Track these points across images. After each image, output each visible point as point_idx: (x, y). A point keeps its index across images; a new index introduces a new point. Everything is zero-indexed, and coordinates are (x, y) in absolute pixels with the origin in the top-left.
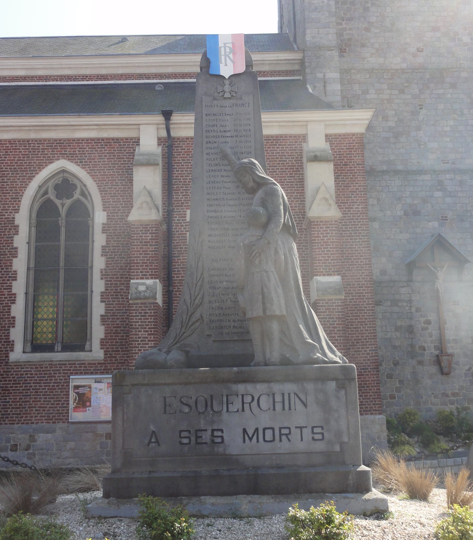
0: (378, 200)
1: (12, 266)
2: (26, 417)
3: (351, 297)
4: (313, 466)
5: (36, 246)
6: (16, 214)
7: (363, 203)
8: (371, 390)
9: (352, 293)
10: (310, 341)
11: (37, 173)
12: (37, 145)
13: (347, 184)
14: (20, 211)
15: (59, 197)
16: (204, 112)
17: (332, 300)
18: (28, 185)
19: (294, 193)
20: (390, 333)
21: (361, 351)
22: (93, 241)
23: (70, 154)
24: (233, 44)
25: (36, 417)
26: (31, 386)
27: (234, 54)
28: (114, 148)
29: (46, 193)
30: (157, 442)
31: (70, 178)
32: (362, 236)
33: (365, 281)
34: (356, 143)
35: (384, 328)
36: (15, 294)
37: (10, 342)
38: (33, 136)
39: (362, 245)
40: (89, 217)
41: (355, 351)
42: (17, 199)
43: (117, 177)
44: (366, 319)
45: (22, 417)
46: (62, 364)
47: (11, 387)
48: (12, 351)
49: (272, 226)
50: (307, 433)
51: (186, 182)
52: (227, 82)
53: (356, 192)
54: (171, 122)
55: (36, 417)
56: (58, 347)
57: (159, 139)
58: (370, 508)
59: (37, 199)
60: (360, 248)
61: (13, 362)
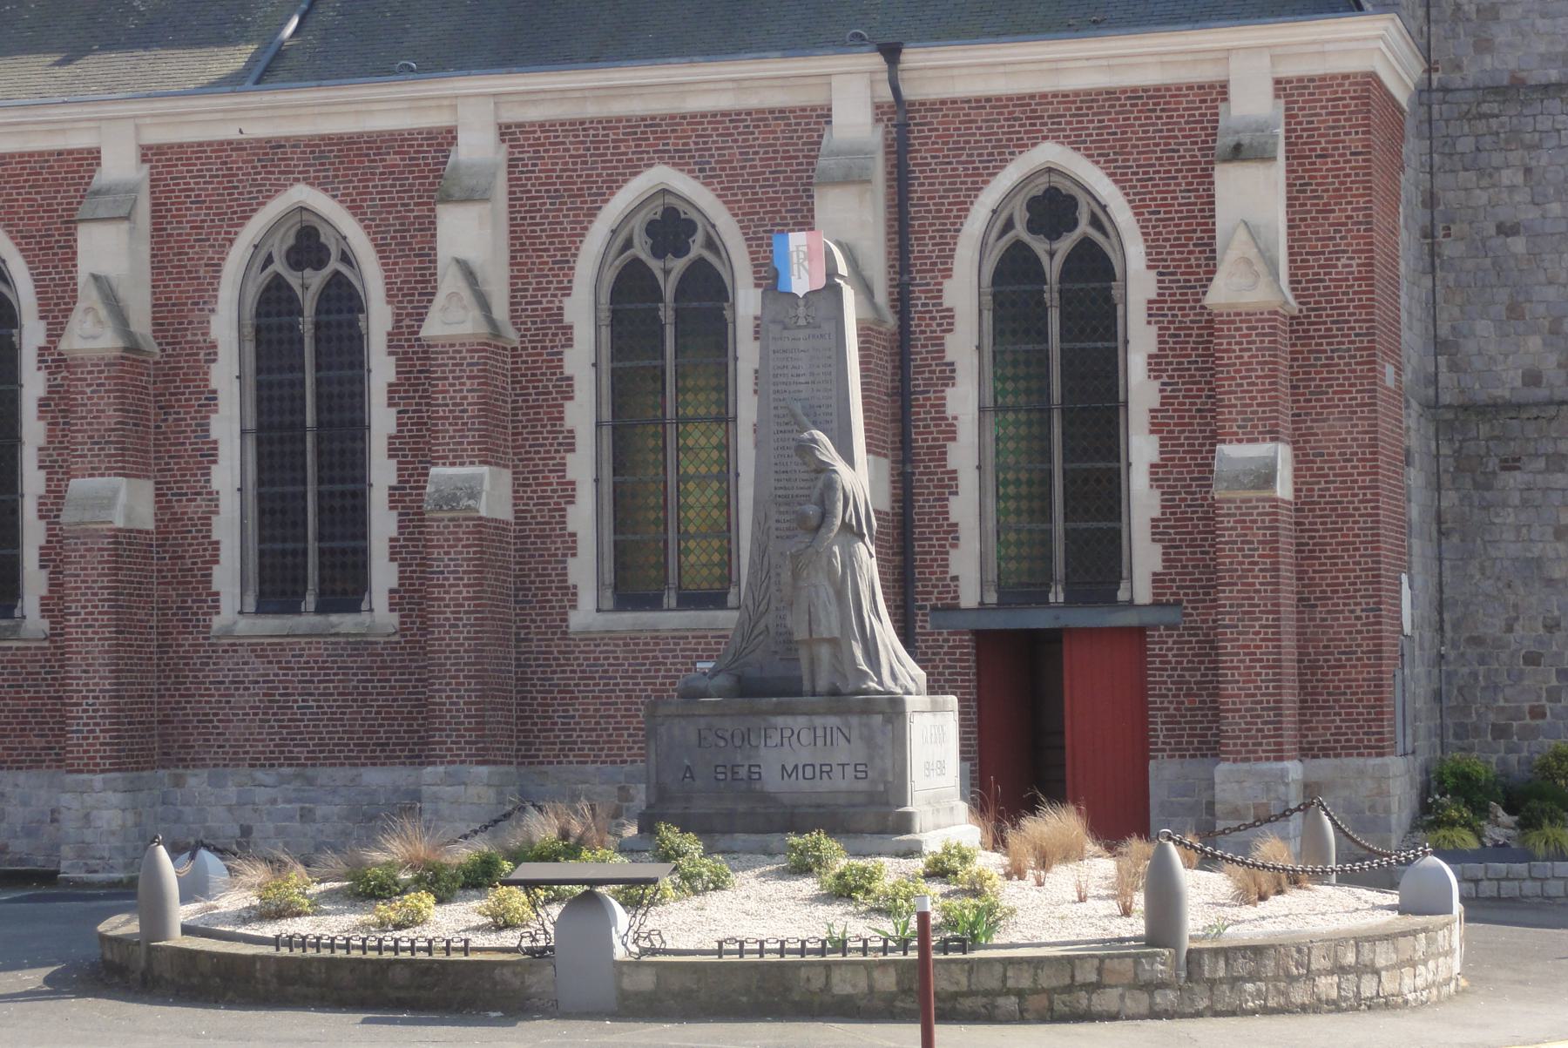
0: (1528, 171)
1: (562, 419)
2: (610, 749)
3: (1323, 485)
4: (853, 806)
5: (613, 370)
6: (565, 299)
7: (1362, 251)
8: (1361, 700)
9: (1327, 475)
10: (865, 668)
11: (606, 201)
12: (601, 132)
13: (1325, 205)
14: (574, 292)
15: (658, 252)
16: (772, 348)
17: (1250, 501)
18: (586, 229)
19: (1195, 231)
20: (1541, 545)
21: (1342, 612)
22: (736, 359)
23: (676, 151)
24: (809, 247)
25: (630, 749)
26: (617, 684)
27: (810, 261)
28: (774, 132)
29: (628, 244)
30: (692, 777)
31: (681, 207)
32: (1357, 335)
33: (1359, 446)
34: (1352, 98)
35: (1524, 530)
36: (573, 483)
37: (567, 588)
38: (592, 110)
39: (1354, 357)
40: (727, 300)
41: (1329, 612)
42: (566, 264)
43: (784, 205)
44: (1358, 536)
45: (602, 749)
46: (679, 637)
47: (577, 685)
48: (574, 607)
49: (823, 530)
50: (849, 770)
51: (940, 211)
52: (801, 303)
53: (1345, 224)
54: (900, 66)
55: (630, 749)
56: (671, 599)
57: (877, 107)
58: (903, 848)
59: (610, 259)
60: (1349, 364)
61: (577, 633)
